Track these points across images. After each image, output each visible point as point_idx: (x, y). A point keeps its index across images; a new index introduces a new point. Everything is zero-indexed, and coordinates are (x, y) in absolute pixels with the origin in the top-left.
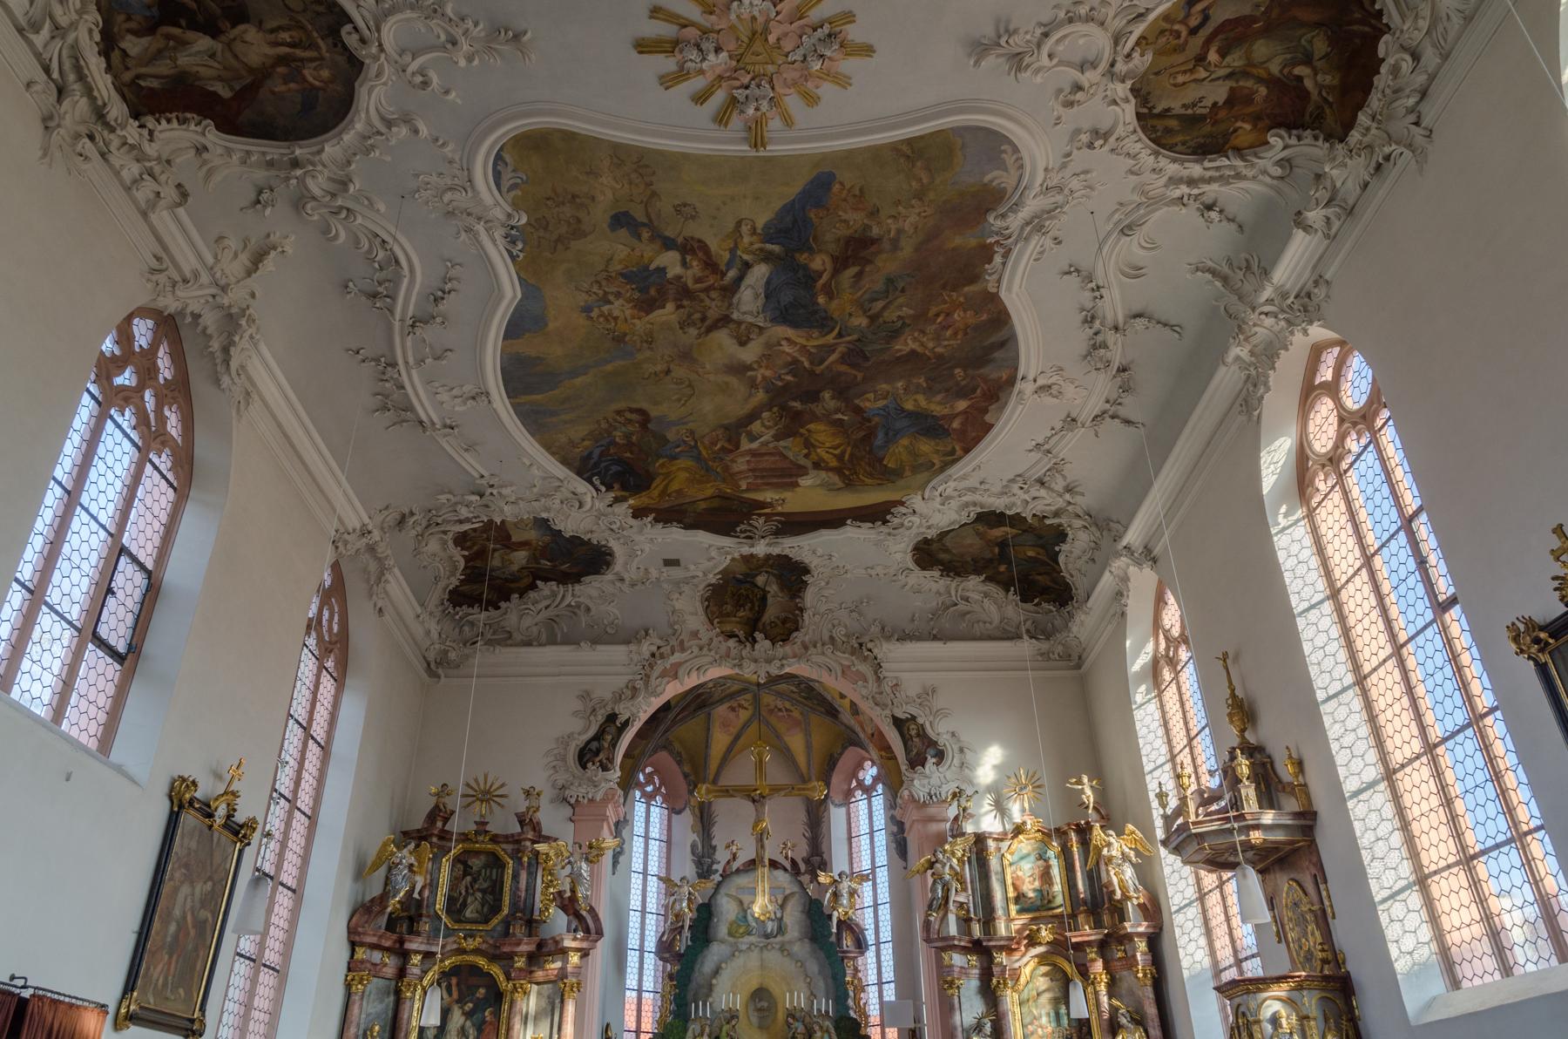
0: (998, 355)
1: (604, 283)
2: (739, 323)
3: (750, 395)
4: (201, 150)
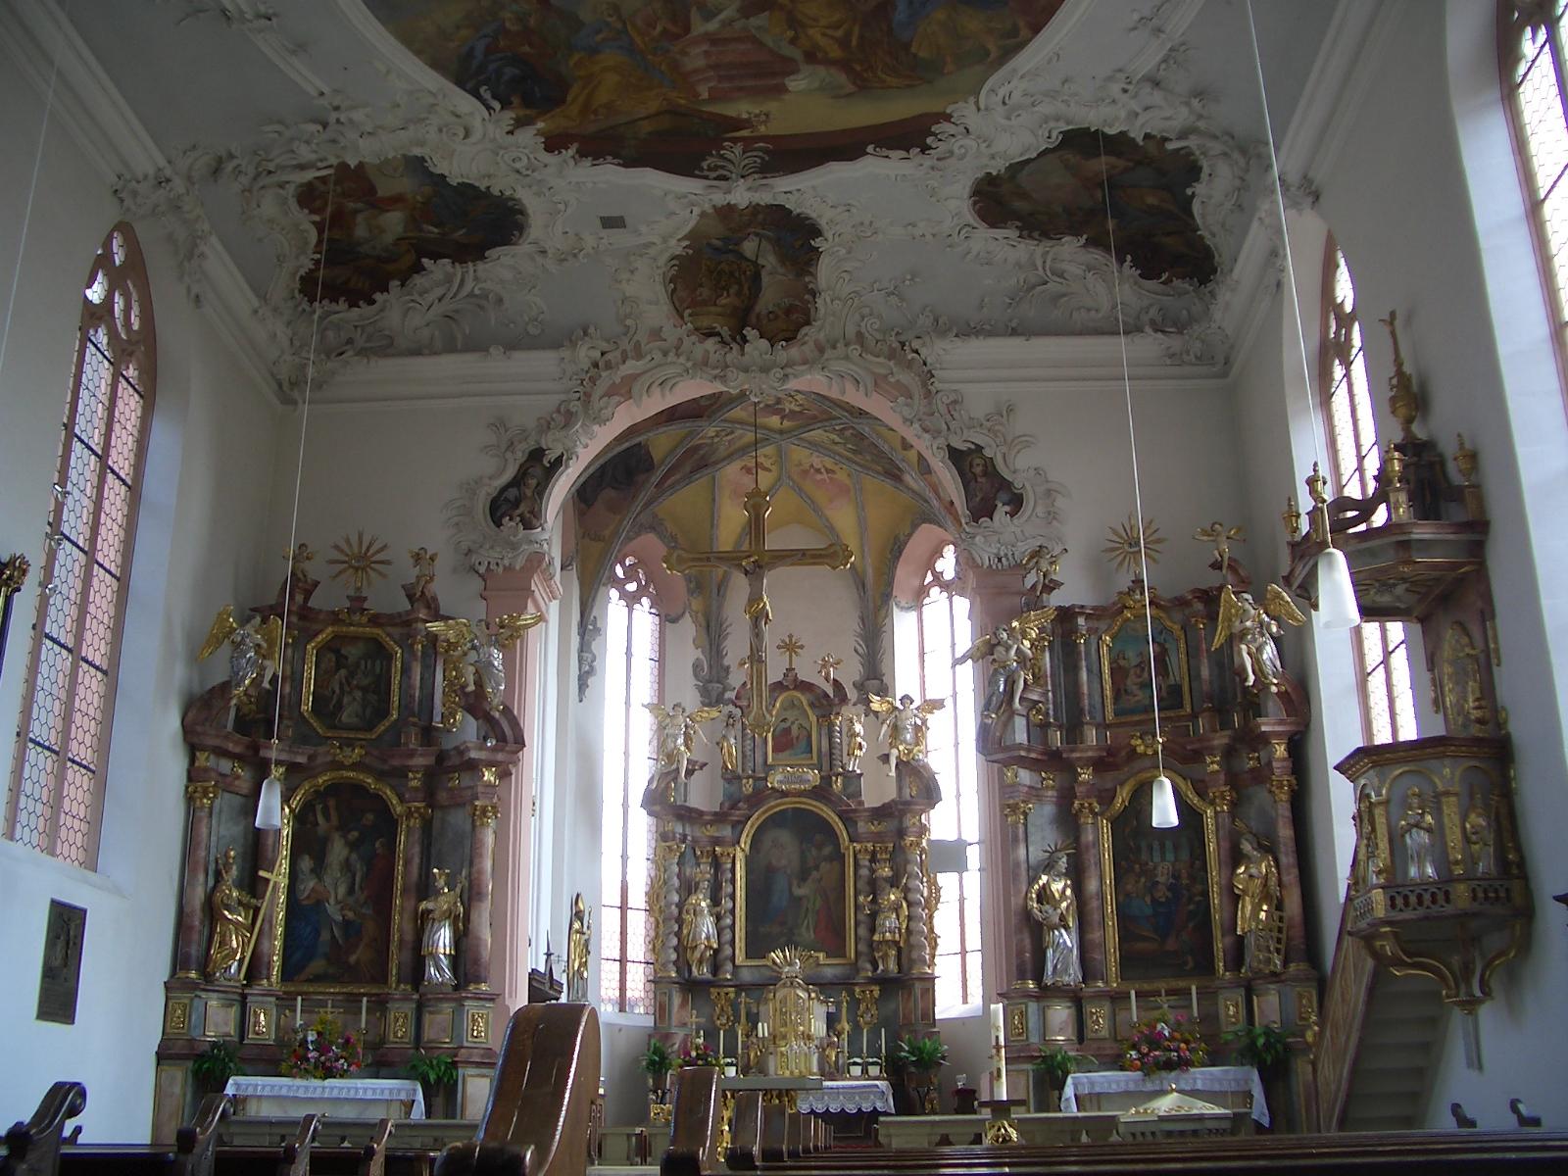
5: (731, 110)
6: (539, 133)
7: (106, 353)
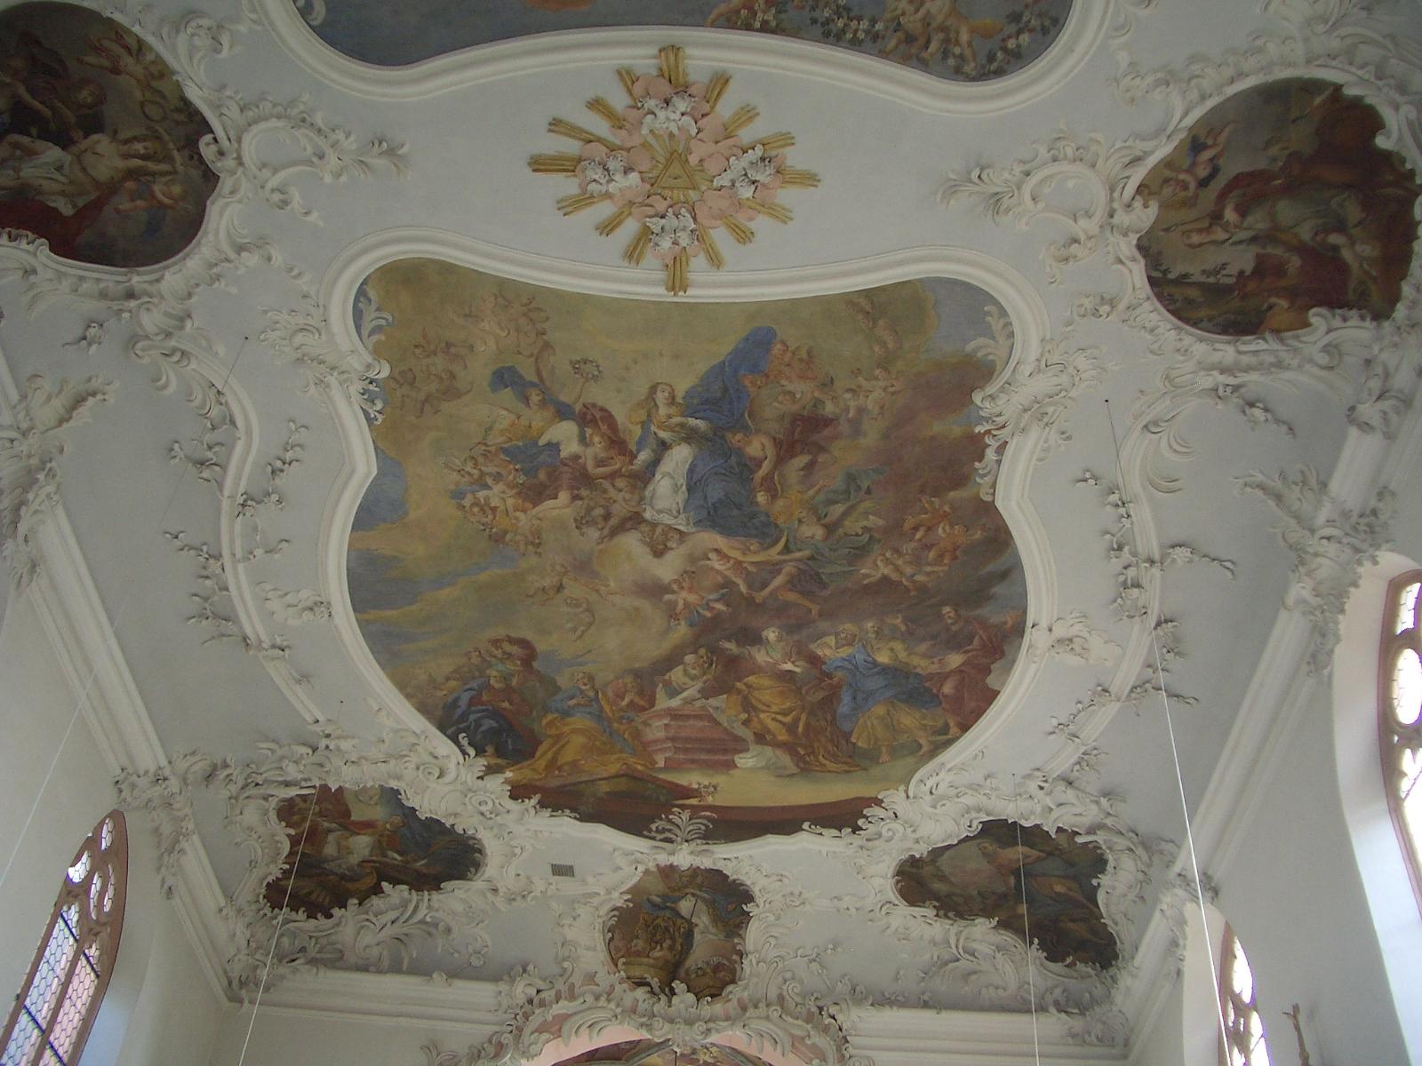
0: (997, 589)
1: (481, 460)
2: (654, 525)
3: (668, 629)
4: (29, 272)
6: (507, 781)
7: (74, 930)
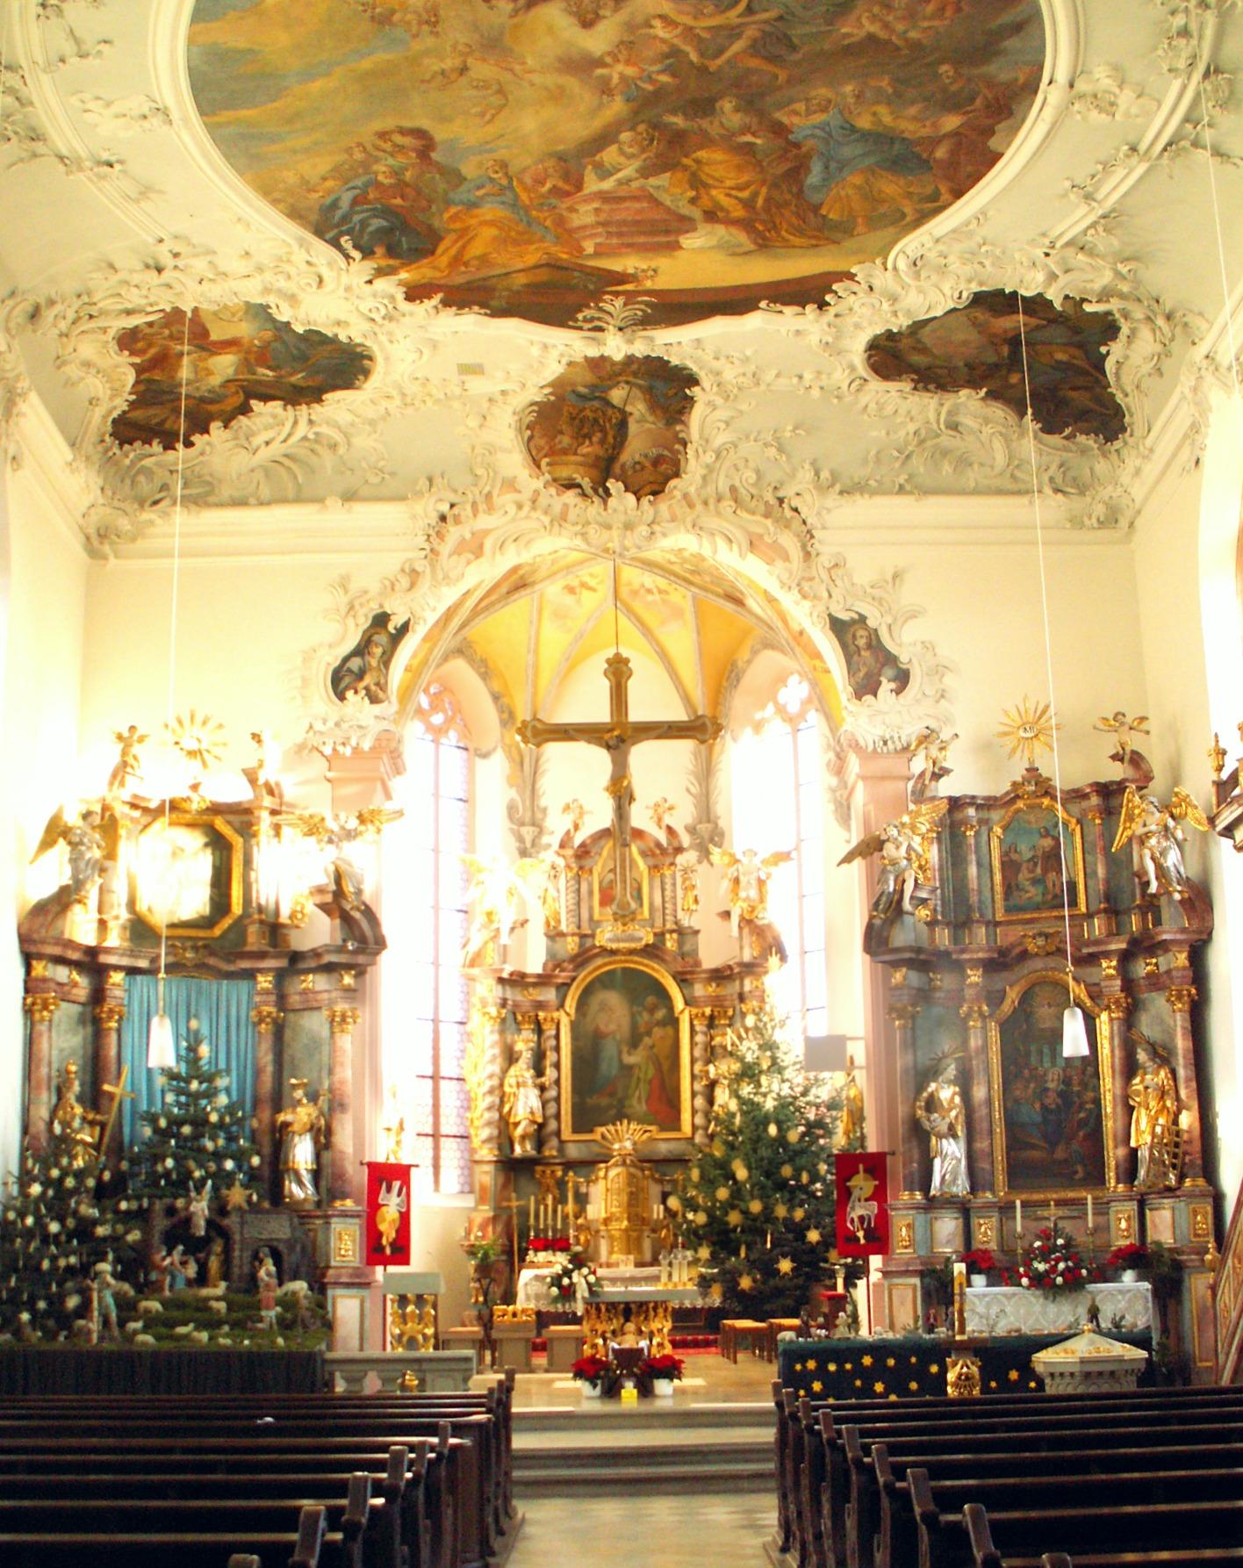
0: (1012, 43)
3: (600, 106)
5: (616, 265)
